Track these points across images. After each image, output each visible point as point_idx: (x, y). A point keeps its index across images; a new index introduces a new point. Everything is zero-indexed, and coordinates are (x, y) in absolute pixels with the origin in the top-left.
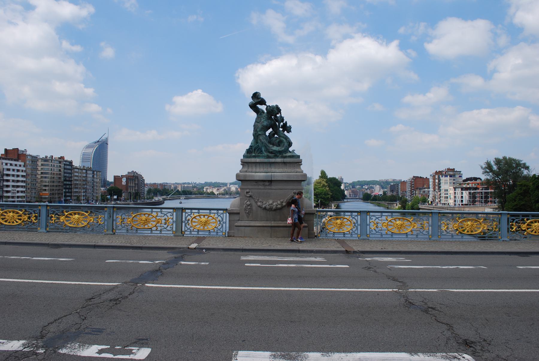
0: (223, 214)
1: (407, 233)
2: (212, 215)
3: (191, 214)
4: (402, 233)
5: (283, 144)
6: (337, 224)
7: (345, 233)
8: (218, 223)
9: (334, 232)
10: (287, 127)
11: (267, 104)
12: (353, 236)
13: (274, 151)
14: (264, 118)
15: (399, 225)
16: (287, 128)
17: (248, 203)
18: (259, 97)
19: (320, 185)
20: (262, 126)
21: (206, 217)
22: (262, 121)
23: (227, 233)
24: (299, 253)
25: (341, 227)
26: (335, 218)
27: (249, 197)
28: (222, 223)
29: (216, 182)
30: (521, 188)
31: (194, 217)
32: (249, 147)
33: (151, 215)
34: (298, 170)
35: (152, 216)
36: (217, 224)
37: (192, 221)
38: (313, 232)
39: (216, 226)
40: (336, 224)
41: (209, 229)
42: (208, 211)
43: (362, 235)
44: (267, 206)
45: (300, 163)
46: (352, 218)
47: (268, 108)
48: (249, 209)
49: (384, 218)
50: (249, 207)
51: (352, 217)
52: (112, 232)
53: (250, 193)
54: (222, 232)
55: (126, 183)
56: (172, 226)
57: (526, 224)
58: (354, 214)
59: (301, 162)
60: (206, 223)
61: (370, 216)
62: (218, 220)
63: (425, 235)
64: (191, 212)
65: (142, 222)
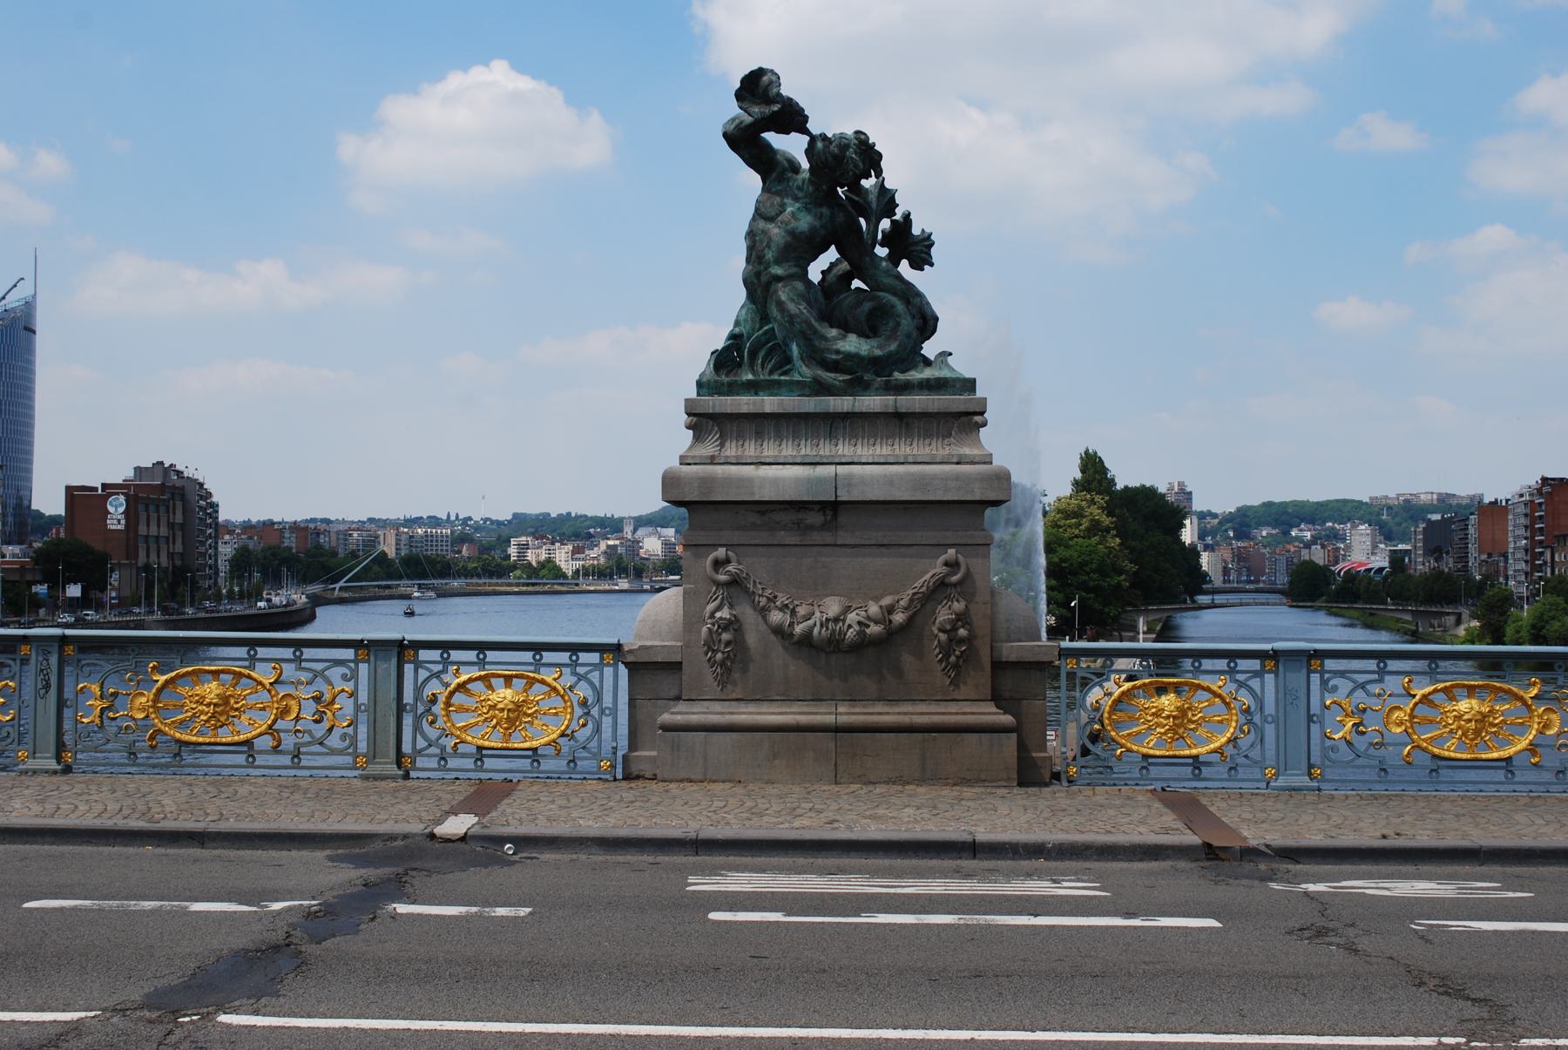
1: (535, 750)
3: (445, 671)
6: (202, 703)
7: (1201, 759)
8: (579, 711)
9: (480, 748)
11: (814, 127)
15: (1469, 721)
17: (724, 613)
21: (519, 684)
23: (620, 760)
24: (974, 857)
25: (1181, 731)
26: (1151, 683)
27: (728, 584)
28: (595, 712)
29: (569, 514)
31: (462, 687)
33: (249, 677)
34: (967, 451)
37: (448, 704)
39: (568, 727)
40: (197, 702)
42: (528, 656)
43: (1282, 770)
44: (816, 631)
45: (977, 418)
47: (820, 145)
48: (728, 643)
49: (1393, 684)
51: (574, 673)
52: (1307, 777)
55: (127, 518)
56: (350, 730)
58: (584, 657)
59: (982, 413)
60: (516, 715)
61: (1327, 676)
63: (333, 752)
64: (446, 662)
65: (202, 712)
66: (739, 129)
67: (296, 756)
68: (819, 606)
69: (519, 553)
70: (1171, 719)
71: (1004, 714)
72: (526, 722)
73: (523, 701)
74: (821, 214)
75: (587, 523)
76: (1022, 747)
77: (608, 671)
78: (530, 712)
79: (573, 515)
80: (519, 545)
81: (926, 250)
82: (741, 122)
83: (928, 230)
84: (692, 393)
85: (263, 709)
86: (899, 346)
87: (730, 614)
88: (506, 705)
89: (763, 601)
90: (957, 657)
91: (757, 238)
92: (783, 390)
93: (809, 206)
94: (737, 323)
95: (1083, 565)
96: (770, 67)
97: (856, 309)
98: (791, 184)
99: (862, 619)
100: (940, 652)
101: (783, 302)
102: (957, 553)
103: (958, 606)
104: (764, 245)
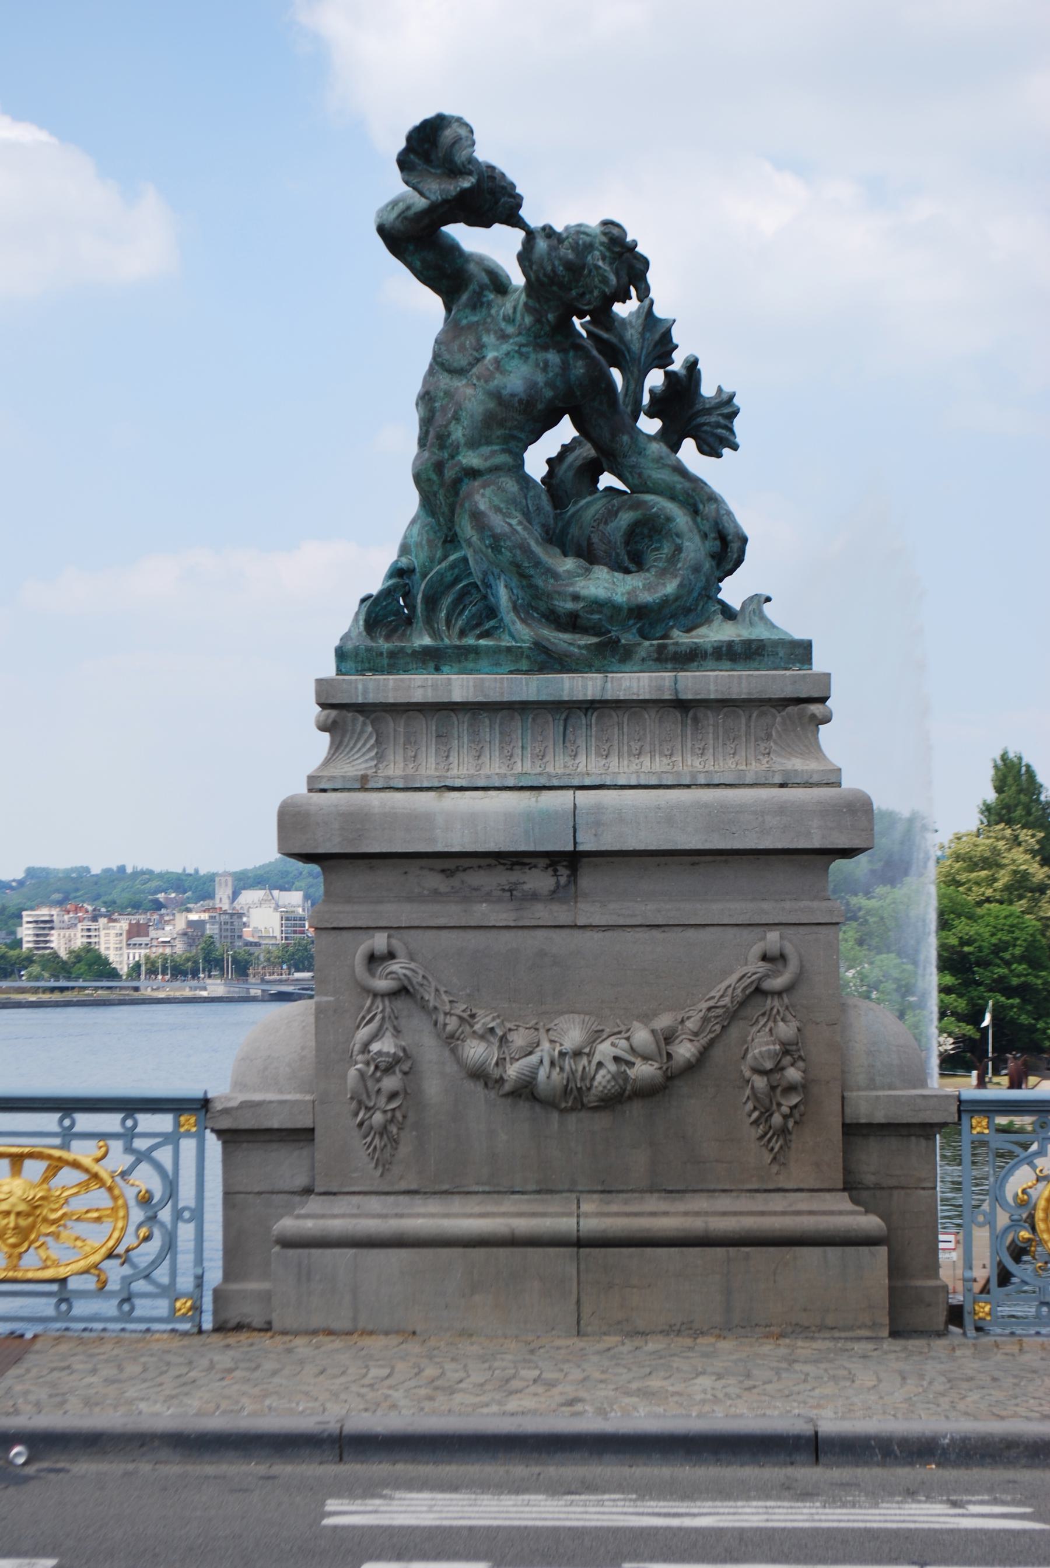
0: (172, 1139)
1: (63, 1281)
2: (83, 1151)
4: (30, 1275)
5: (667, 549)
8: (137, 1215)
10: (699, 407)
11: (532, 214)
12: (143, 1307)
13: (597, 605)
17: (386, 1045)
18: (461, 157)
19: (992, 880)
21: (34, 1169)
22: (491, 355)
28: (165, 1215)
35: (84, 1177)
36: (124, 1229)
38: (931, 1283)
39: (119, 1241)
41: (62, 1272)
42: (49, 1121)
44: (542, 1074)
46: (130, 1159)
47: (542, 245)
50: (390, 1083)
51: (129, 1149)
53: (395, 967)
54: (169, 1291)
59: (823, 700)
62: (130, 1194)
67: (128, 1299)
68: (548, 1030)
69: (37, 935)
70: (12, 1217)
71: (867, 1212)
72: (48, 1235)
73: (42, 1198)
74: (546, 363)
75: (154, 884)
76: (896, 1269)
77: (189, 1146)
78: (54, 1216)
79: (129, 870)
80: (36, 922)
81: (722, 421)
82: (408, 208)
84: (329, 669)
85: (98, 1220)
86: (681, 586)
87: (396, 1046)
88: (14, 1205)
89: (452, 1023)
90: (785, 1117)
91: (437, 405)
92: (484, 663)
93: (524, 350)
94: (404, 549)
95: (998, 949)
97: (606, 523)
98: (493, 311)
99: (619, 1053)
100: (755, 1109)
102: (389, 937)
103: (786, 1030)
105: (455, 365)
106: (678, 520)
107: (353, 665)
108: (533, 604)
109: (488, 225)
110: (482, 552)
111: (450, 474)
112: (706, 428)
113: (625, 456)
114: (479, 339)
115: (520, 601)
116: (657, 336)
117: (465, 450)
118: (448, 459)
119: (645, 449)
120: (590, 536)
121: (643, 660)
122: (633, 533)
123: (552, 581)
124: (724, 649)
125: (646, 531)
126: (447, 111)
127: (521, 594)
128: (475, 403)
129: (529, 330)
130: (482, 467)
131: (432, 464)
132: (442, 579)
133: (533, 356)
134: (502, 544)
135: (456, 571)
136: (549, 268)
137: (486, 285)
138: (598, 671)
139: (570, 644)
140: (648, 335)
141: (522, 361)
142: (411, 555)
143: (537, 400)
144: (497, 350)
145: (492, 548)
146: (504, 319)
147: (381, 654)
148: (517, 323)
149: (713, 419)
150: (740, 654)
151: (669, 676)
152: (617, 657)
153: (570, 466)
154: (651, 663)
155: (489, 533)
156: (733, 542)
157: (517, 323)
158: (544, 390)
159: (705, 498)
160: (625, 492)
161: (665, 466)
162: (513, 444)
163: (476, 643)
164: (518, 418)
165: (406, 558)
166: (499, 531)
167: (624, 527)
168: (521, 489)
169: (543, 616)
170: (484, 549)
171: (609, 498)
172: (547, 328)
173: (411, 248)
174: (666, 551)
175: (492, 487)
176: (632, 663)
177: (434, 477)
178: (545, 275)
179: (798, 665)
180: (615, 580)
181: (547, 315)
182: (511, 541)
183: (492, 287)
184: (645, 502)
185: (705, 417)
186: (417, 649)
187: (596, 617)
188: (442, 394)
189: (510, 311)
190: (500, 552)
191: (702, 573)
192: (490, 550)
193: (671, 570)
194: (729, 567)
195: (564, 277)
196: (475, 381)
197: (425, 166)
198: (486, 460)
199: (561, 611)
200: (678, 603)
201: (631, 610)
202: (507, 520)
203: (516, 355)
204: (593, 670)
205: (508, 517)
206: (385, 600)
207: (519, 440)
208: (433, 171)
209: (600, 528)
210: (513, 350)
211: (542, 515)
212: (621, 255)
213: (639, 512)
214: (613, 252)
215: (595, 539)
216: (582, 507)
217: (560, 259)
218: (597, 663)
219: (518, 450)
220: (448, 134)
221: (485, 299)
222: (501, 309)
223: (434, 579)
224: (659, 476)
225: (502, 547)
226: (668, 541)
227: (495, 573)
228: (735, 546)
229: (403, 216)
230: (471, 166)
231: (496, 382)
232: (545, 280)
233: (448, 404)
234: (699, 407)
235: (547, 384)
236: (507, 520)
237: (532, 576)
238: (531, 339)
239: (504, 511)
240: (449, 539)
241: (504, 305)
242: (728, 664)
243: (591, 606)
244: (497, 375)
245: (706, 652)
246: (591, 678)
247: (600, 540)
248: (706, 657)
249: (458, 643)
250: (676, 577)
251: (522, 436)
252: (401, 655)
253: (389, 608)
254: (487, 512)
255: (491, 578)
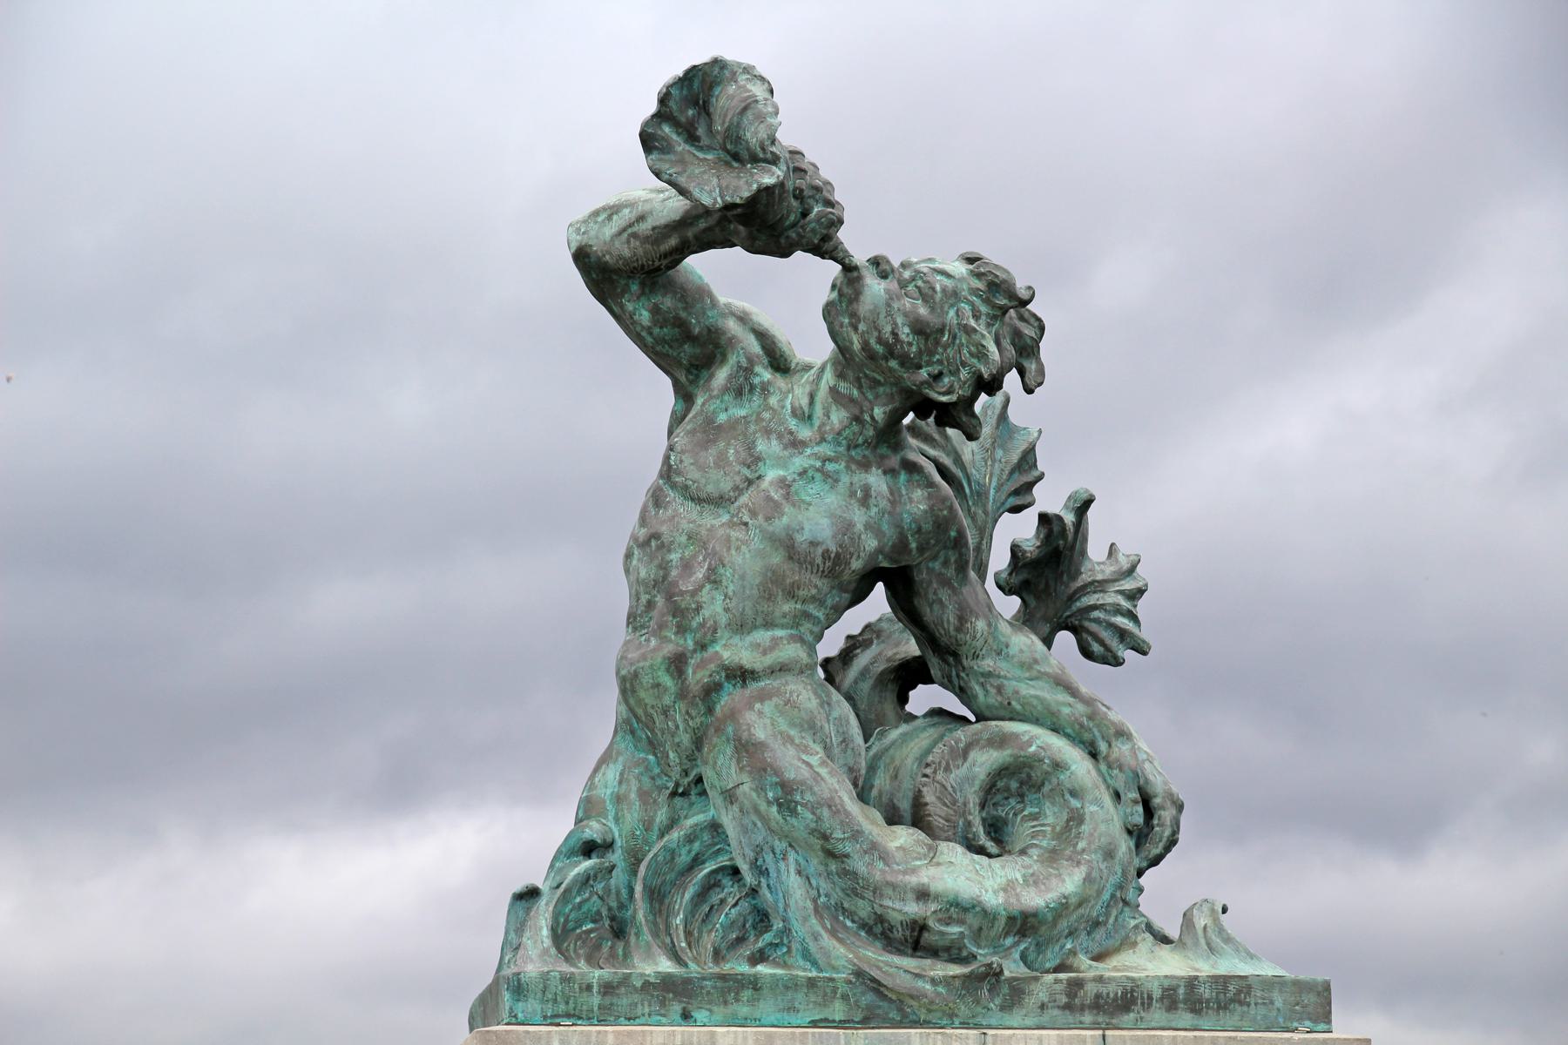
5: (1052, 816)
10: (1085, 577)
11: (856, 240)
13: (958, 908)
14: (796, 444)
16: (1084, 590)
18: (753, 135)
20: (777, 559)
22: (771, 474)
30: (966, 933)
32: (1160, 925)
47: (875, 287)
57: (566, 968)
66: (635, 235)
74: (867, 491)
81: (1125, 604)
82: (641, 218)
83: (1126, 550)
86: (1088, 879)
91: (674, 557)
92: (767, 1008)
93: (830, 467)
94: (588, 808)
96: (745, 59)
97: (947, 769)
98: (773, 401)
101: (761, 746)
104: (700, 574)
105: (710, 488)
106: (1073, 768)
107: (538, 1007)
108: (846, 905)
109: (785, 253)
110: (757, 811)
111: (698, 676)
112: (1096, 614)
113: (976, 656)
114: (750, 447)
115: (823, 899)
116: (1015, 457)
117: (727, 635)
118: (695, 651)
119: (1007, 646)
120: (920, 791)
121: (1043, 1007)
122: (992, 790)
123: (881, 865)
124: (1181, 991)
125: (1014, 785)
126: (730, 55)
127: (824, 886)
128: (748, 556)
129: (839, 434)
130: (758, 666)
131: (664, 658)
132: (673, 859)
133: (845, 479)
134: (798, 798)
135: (697, 846)
136: (888, 329)
137: (758, 356)
138: (965, 1025)
139: (917, 976)
140: (999, 453)
141: (827, 487)
142: (606, 818)
143: (852, 555)
144: (784, 466)
145: (780, 805)
146: (794, 413)
147: (589, 988)
148: (817, 423)
149: (1111, 598)
150: (1208, 1001)
151: (974, 1034)
152: (998, 1001)
153: (864, 673)
154: (1056, 1012)
155: (775, 779)
156: (1163, 808)
157: (817, 423)
158: (863, 537)
159: (1112, 731)
160: (964, 720)
161: (1040, 676)
162: (807, 626)
163: (753, 971)
164: (819, 583)
165: (598, 821)
166: (792, 776)
167: (982, 776)
168: (821, 705)
169: (864, 926)
170: (763, 807)
171: (941, 729)
172: (870, 432)
173: (635, 288)
174: (1050, 820)
175: (775, 699)
176: (1024, 1011)
177: (667, 681)
178: (880, 341)
179: (1308, 1023)
180: (978, 867)
181: (872, 410)
182: (813, 793)
183: (766, 361)
184: (1015, 736)
185: (1096, 596)
186: (652, 980)
187: (955, 929)
188: (684, 539)
189: (805, 402)
190: (794, 812)
191: (1117, 861)
192: (774, 809)
193: (1067, 852)
194: (1156, 851)
195: (910, 344)
196: (746, 518)
197: (687, 147)
198: (764, 653)
199: (895, 917)
200: (1081, 911)
201: (1011, 919)
202: (804, 757)
203: (818, 476)
204: (957, 1021)
205: (804, 752)
206: (579, 893)
207: (816, 620)
208: (701, 155)
209: (939, 777)
210: (811, 466)
211: (849, 751)
212: (1004, 310)
213: (1008, 752)
214: (994, 306)
215: (929, 797)
216: (893, 743)
217: (906, 315)
218: (963, 1010)
219: (811, 639)
220: (725, 100)
221: (756, 380)
222: (787, 397)
223: (660, 858)
224: (1032, 692)
225: (797, 803)
226: (1053, 804)
227: (778, 851)
228: (1166, 815)
229: (630, 231)
230: (764, 156)
231: (785, 520)
232: (880, 349)
233: (694, 556)
234: (1085, 577)
235: (868, 526)
236: (804, 757)
237: (847, 856)
238: (841, 449)
239: (797, 741)
240: (680, 790)
241: (791, 390)
242: (1186, 1018)
243: (948, 910)
244: (787, 509)
245: (1150, 998)
246: (958, 1037)
247: (939, 798)
248: (1150, 1005)
249: (716, 970)
250: (1079, 863)
251: (820, 615)
252: (623, 990)
253: (585, 908)
254: (770, 742)
255: (769, 858)
